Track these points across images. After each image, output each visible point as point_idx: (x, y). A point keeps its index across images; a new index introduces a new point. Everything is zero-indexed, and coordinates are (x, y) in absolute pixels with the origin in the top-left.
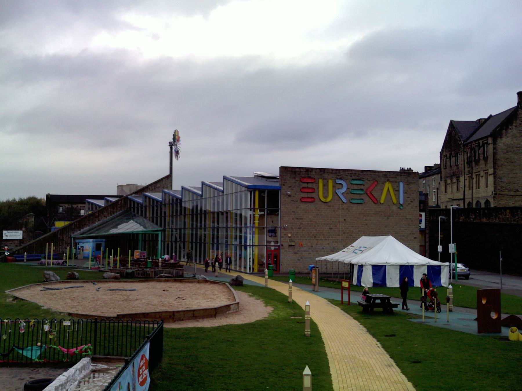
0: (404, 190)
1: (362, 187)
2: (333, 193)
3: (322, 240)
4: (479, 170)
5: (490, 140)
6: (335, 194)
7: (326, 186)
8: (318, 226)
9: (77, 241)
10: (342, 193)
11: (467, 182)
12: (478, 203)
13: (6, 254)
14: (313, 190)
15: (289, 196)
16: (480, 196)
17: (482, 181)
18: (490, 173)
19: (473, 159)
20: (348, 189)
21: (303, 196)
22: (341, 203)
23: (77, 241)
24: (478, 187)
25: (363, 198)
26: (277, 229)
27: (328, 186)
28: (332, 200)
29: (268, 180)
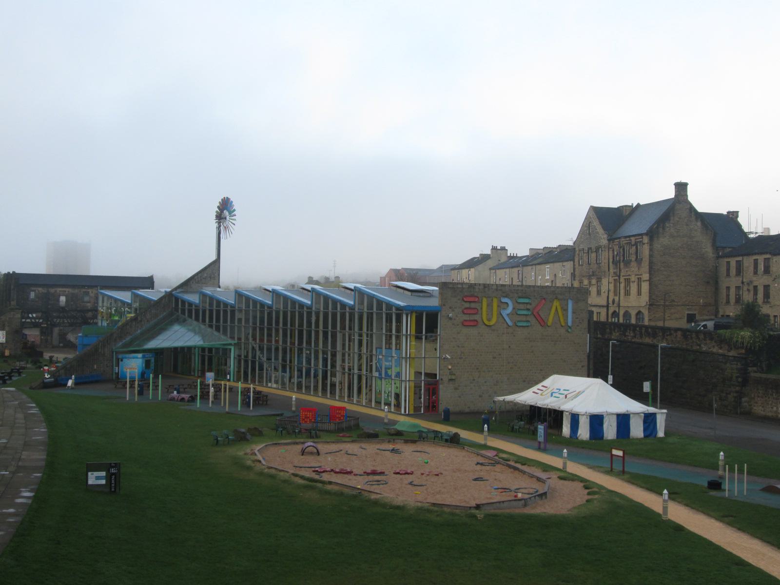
0: (573, 310)
1: (529, 307)
2: (498, 314)
3: (484, 372)
4: (629, 273)
5: (646, 239)
7: (490, 305)
8: (481, 355)
9: (120, 356)
10: (508, 315)
11: (612, 286)
12: (627, 314)
13: (46, 376)
14: (476, 311)
15: (450, 319)
16: (630, 305)
17: (634, 288)
18: (645, 279)
19: (622, 259)
20: (514, 308)
21: (466, 319)
22: (505, 325)
23: (120, 356)
25: (530, 319)
27: (492, 306)
28: (496, 323)
29: (414, 294)
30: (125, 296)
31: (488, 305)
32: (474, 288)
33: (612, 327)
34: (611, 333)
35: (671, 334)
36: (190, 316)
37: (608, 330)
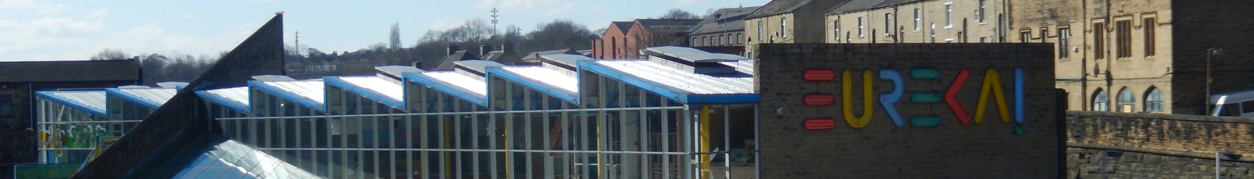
6: (878, 105)
7: (858, 88)
11: (1091, 39)
17: (1138, 38)
20: (906, 91)
24: (1124, 50)
26: (707, 150)
30: (95, 100)
31: (854, 87)
32: (825, 54)
33: (1099, 121)
34: (1095, 135)
35: (1225, 132)
36: (399, 123)
37: (1090, 129)
